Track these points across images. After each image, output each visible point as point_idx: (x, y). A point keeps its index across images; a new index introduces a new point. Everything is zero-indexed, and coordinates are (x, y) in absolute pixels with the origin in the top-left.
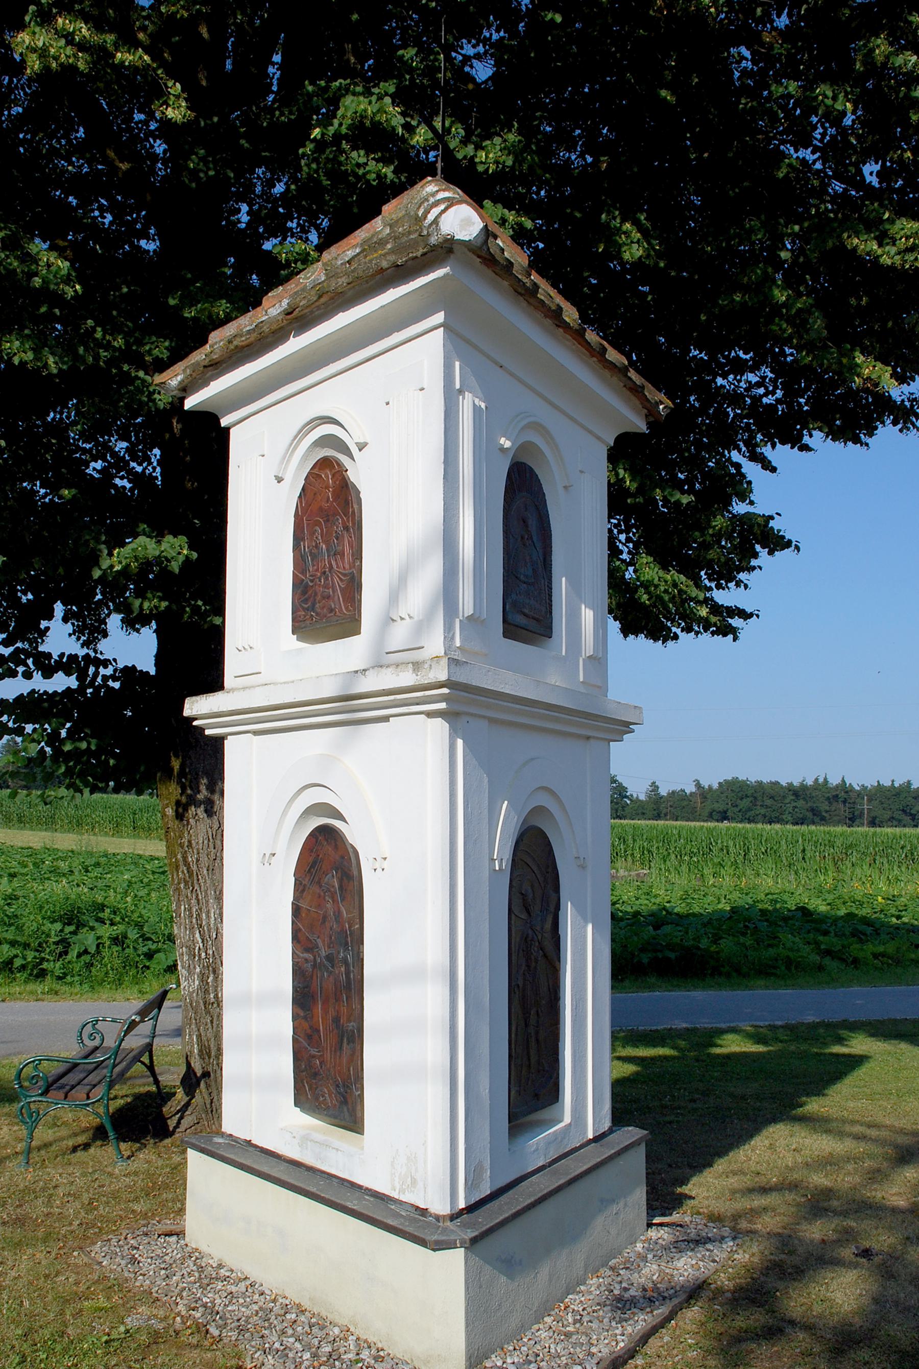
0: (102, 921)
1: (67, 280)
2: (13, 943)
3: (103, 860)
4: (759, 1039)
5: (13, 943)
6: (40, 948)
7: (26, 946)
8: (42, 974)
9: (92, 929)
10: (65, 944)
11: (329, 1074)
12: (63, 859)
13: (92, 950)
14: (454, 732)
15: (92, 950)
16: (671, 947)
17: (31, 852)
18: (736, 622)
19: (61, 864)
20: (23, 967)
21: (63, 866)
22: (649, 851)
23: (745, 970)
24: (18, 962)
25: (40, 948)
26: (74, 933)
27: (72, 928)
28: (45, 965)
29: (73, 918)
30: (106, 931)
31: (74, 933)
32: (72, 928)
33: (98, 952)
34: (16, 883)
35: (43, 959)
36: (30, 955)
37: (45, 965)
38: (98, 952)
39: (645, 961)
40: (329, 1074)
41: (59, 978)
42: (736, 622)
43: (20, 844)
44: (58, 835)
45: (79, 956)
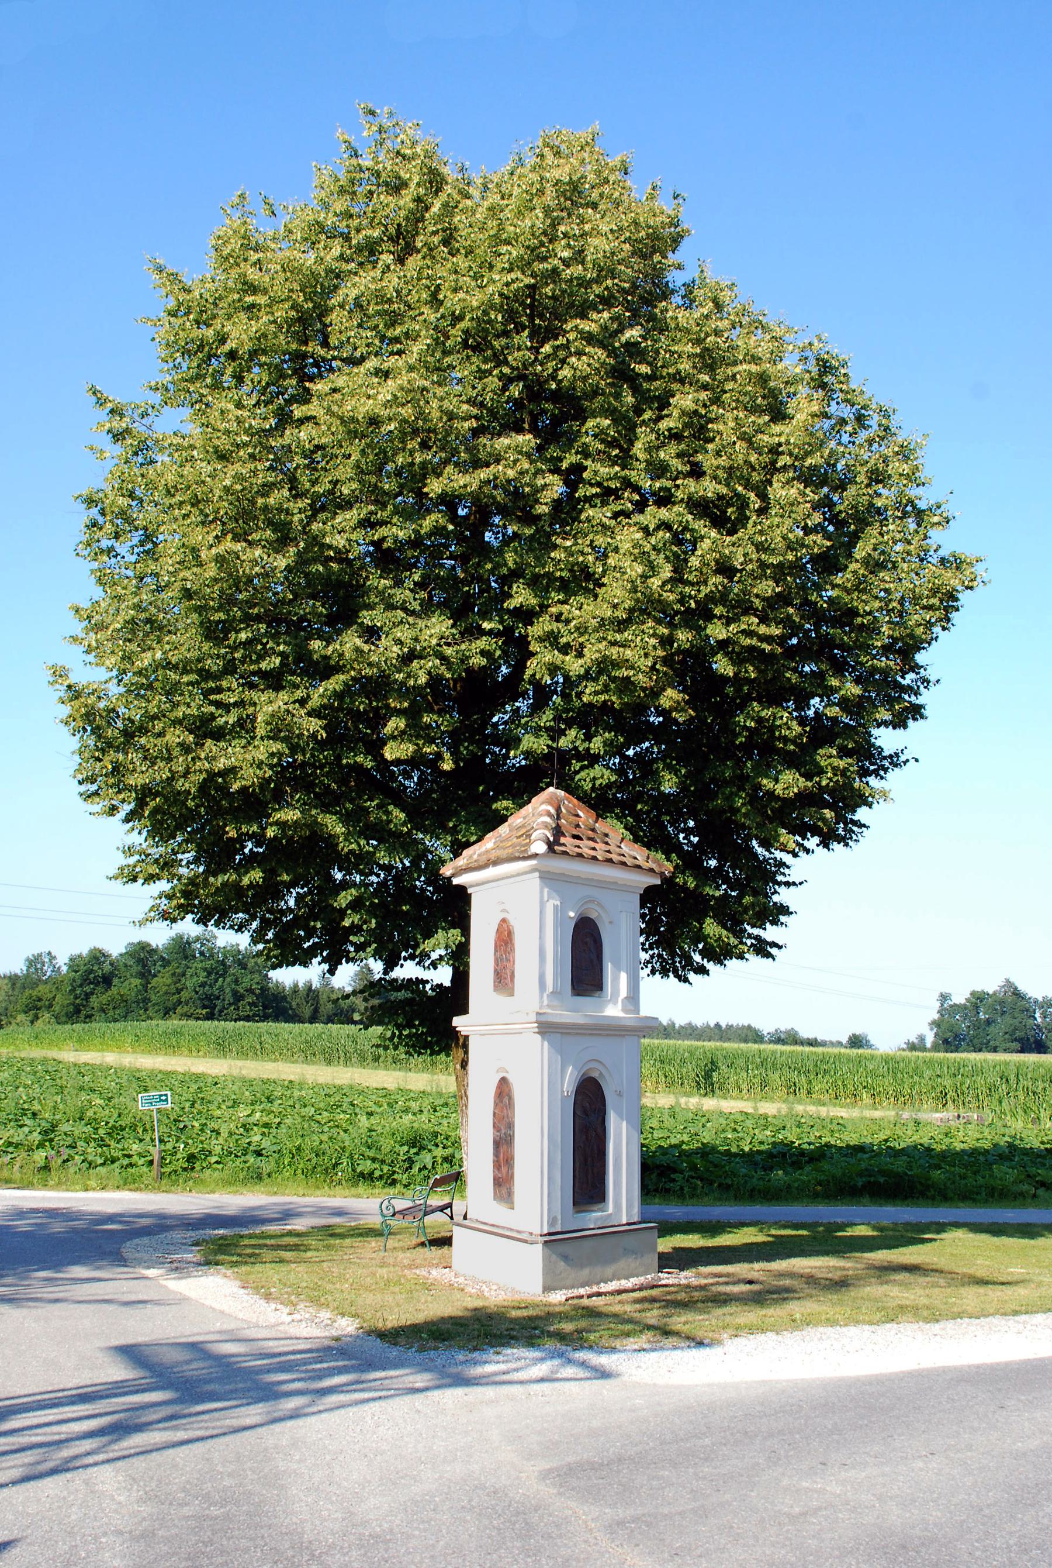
0: (437, 1145)
1: (404, 824)
2: (374, 1160)
3: (451, 1101)
4: (874, 1228)
5: (374, 1160)
6: (392, 1164)
7: (383, 1162)
8: (394, 1182)
9: (430, 1151)
10: (411, 1161)
11: (503, 1183)
12: (415, 1100)
13: (429, 1166)
14: (543, 1038)
15: (429, 1166)
16: (881, 1172)
17: (386, 1093)
18: (774, 951)
19: (413, 1104)
20: (381, 1177)
21: (414, 1106)
22: (1034, 1093)
23: (950, 1195)
24: (377, 1174)
25: (392, 1164)
26: (417, 1154)
27: (415, 1150)
28: (395, 1176)
29: (416, 1142)
30: (439, 1152)
31: (417, 1154)
32: (415, 1150)
33: (433, 1168)
34: (373, 1120)
35: (394, 1172)
36: (386, 1168)
37: (395, 1176)
38: (433, 1168)
39: (860, 1184)
40: (503, 1183)
41: (406, 1186)
42: (774, 951)
43: (375, 1085)
44: (410, 1074)
45: (420, 1170)
